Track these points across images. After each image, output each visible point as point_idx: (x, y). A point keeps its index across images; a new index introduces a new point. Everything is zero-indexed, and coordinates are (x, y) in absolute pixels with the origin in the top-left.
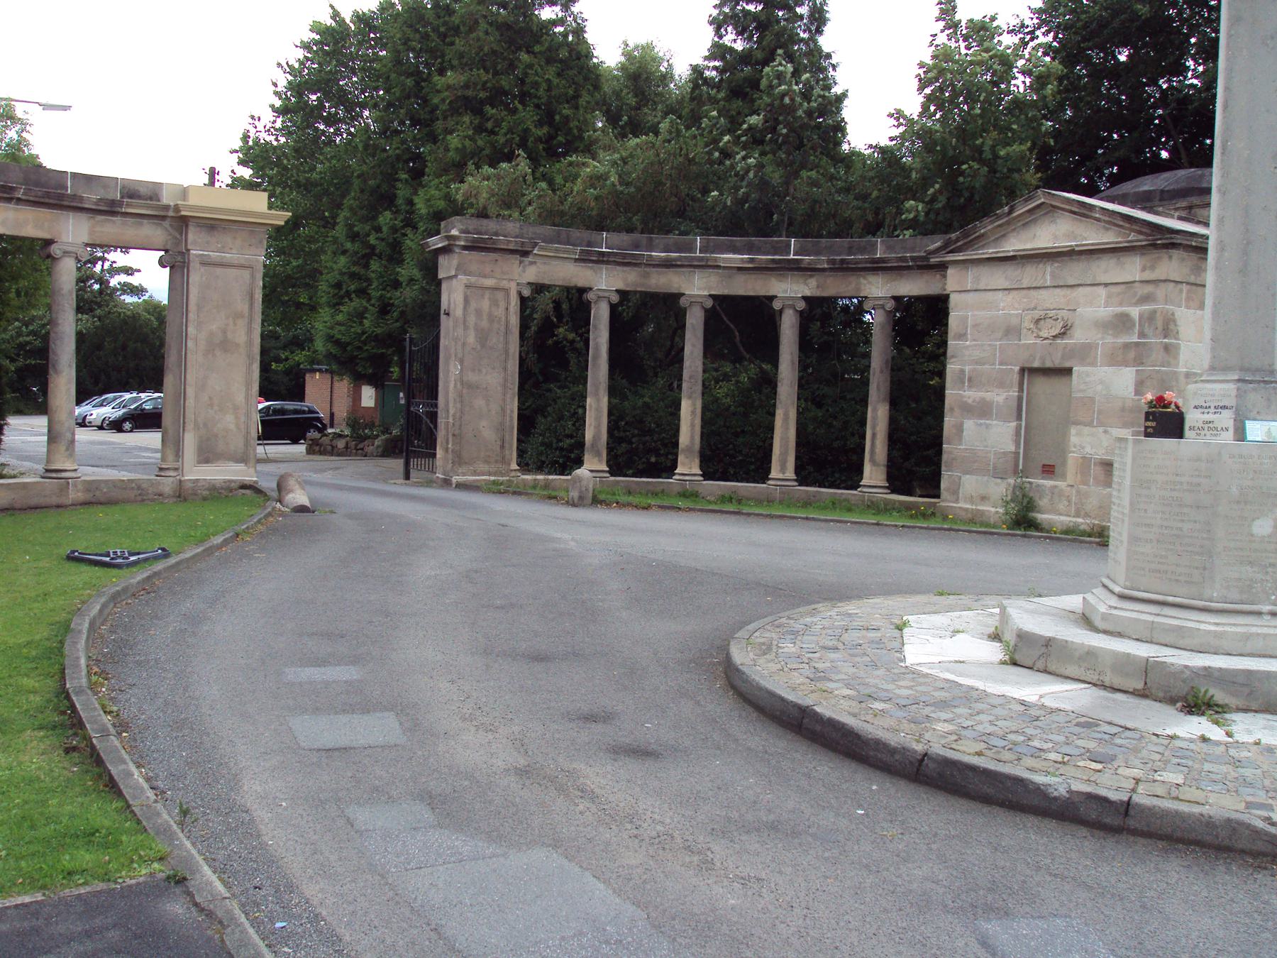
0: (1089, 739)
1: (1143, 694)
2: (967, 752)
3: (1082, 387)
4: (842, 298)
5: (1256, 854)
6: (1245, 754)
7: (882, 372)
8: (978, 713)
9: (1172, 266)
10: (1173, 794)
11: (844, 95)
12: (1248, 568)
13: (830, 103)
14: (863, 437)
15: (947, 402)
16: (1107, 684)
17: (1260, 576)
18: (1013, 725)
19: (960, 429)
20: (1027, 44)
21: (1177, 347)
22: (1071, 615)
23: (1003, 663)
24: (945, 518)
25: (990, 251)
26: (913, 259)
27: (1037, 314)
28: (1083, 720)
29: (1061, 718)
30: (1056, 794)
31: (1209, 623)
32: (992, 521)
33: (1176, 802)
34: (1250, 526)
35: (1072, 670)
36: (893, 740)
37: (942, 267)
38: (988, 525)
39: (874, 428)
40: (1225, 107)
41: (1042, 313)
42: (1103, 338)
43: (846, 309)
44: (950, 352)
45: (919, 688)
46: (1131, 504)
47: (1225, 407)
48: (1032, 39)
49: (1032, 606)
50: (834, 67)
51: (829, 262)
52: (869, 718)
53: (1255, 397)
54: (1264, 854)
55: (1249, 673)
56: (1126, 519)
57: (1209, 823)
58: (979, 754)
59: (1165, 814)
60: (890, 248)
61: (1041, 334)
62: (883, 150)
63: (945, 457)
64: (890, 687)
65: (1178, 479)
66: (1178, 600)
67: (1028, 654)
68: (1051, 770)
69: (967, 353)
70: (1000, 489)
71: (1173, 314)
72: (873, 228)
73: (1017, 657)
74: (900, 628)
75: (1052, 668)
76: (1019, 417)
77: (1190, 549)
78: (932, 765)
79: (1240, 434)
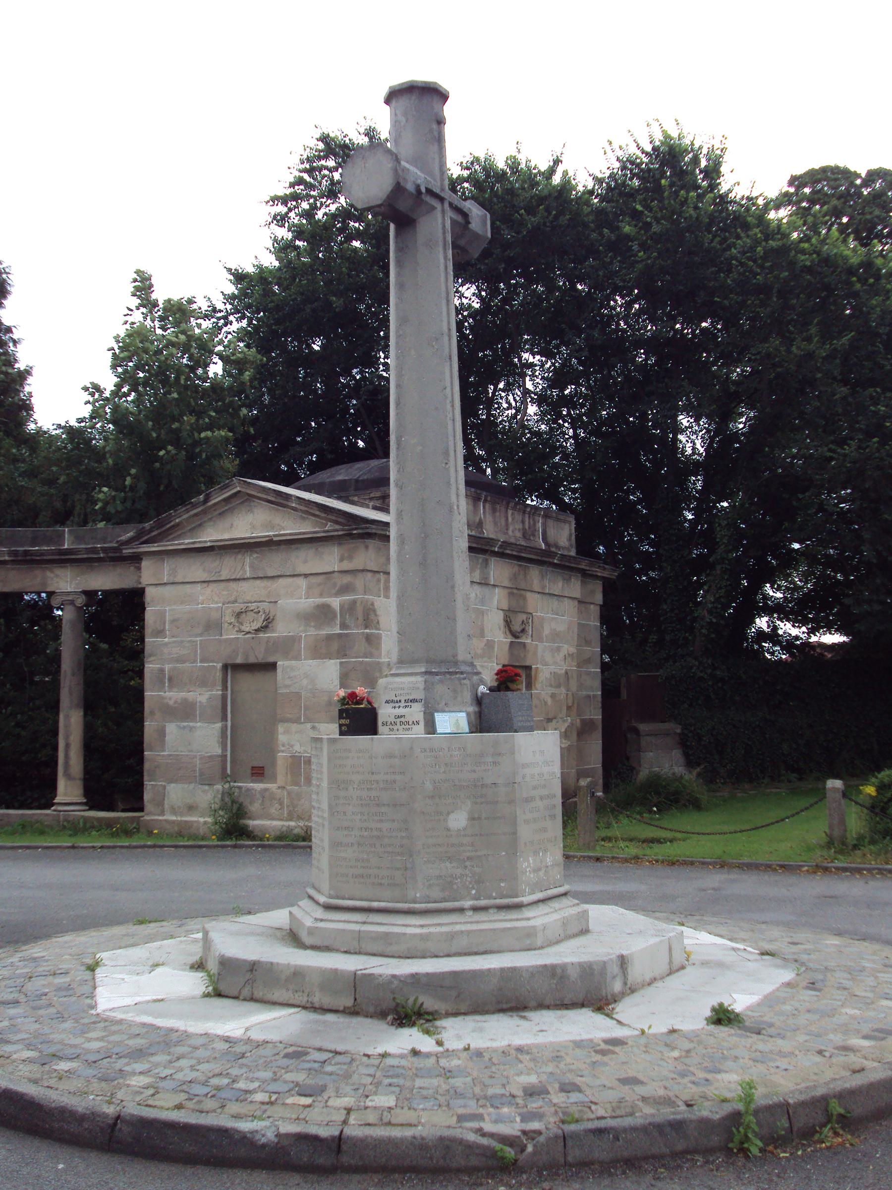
0: (298, 1070)
1: (353, 1012)
2: (165, 1108)
3: (288, 682)
4: (27, 593)
5: (470, 1171)
6: (455, 1062)
7: (73, 675)
8: (178, 1059)
9: (365, 556)
10: (386, 1120)
11: (28, 372)
12: (448, 864)
13: (14, 381)
14: (56, 748)
15: (146, 704)
16: (317, 1005)
17: (459, 871)
18: (216, 1067)
19: (162, 733)
20: (220, 329)
21: (379, 637)
22: (278, 933)
23: (207, 995)
24: (150, 833)
25: (186, 542)
26: (104, 550)
27: (238, 607)
28: (291, 1050)
29: (268, 1051)
30: (264, 1140)
31: (415, 926)
32: (201, 831)
33: (388, 1128)
34: (445, 820)
35: (278, 994)
36: (79, 1104)
37: (136, 559)
38: (195, 837)
39: (67, 737)
40: (398, 404)
41: (242, 606)
42: (305, 631)
43: (33, 605)
44: (148, 648)
45: (111, 1038)
46: (330, 807)
47: (414, 701)
48: (226, 325)
49: (235, 927)
50: (15, 342)
51: (10, 553)
52: (53, 1082)
53: (442, 690)
54: (477, 1169)
55: (455, 974)
56: (326, 823)
57: (421, 1145)
58: (179, 1107)
59: (379, 1143)
60: (79, 539)
61: (243, 628)
62: (70, 431)
63: (147, 766)
64: (78, 1041)
65: (375, 777)
66: (383, 905)
67: (234, 982)
68: (258, 1113)
69: (166, 651)
70: (207, 796)
71: (373, 604)
72: (62, 518)
73: (222, 987)
74: (92, 968)
75: (258, 994)
76: (224, 718)
77: (389, 849)
78: (126, 1129)
79: (431, 727)
